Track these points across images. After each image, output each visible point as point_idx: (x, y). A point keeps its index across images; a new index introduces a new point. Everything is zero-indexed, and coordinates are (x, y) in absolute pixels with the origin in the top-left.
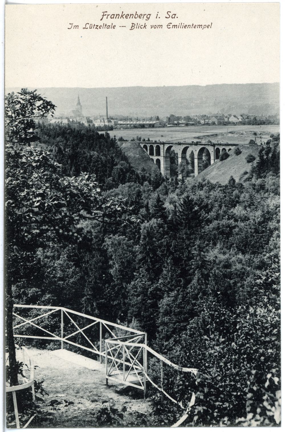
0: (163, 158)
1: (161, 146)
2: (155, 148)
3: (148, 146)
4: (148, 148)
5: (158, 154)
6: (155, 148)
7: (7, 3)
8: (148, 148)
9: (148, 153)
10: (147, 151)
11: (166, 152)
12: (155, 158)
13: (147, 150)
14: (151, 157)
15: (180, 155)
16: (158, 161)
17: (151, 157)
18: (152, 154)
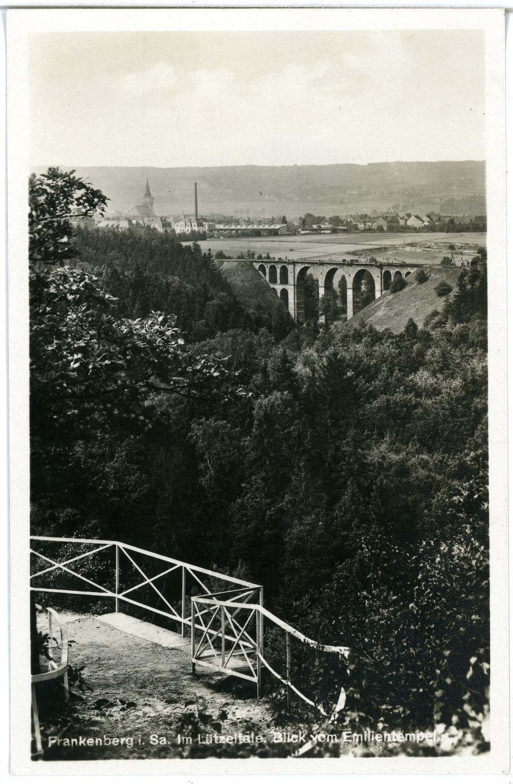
1: (290, 268)
2: (278, 271)
4: (267, 271)
5: (284, 280)
6: (278, 271)
7: (507, 11)
8: (267, 271)
9: (267, 278)
10: (265, 275)
11: (298, 278)
12: (279, 287)
13: (265, 273)
14: (272, 286)
15: (321, 283)
16: (285, 292)
17: (272, 286)
18: (273, 280)
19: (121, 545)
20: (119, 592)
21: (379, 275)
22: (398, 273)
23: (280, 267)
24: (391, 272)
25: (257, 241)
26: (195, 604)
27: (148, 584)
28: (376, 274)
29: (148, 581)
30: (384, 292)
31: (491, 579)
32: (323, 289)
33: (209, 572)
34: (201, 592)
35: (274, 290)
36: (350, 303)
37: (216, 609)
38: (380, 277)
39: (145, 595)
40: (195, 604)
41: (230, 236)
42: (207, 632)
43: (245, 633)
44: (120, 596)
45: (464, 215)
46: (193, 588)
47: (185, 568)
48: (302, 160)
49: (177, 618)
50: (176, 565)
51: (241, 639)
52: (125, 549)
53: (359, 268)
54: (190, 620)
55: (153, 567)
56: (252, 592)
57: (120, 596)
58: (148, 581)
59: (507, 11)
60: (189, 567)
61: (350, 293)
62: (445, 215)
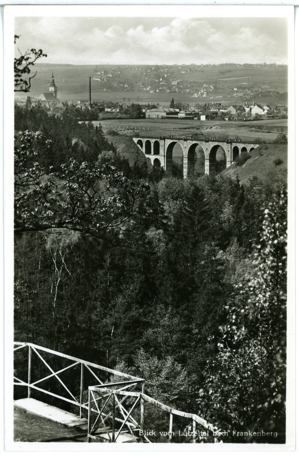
0: (163, 157)
1: (161, 142)
2: (152, 145)
3: (144, 141)
4: (144, 145)
5: (157, 152)
6: (152, 145)
7: (295, 6)
9: (144, 150)
12: (152, 157)
13: (142, 146)
14: (147, 156)
17: (147, 156)
18: (148, 152)
19: (33, 346)
20: (31, 383)
21: (230, 150)
22: (244, 149)
23: (145, 141)
24: (239, 147)
25: (138, 122)
26: (92, 392)
27: (54, 376)
28: (227, 148)
29: (54, 374)
30: (233, 163)
31: (13, 309)
32: (208, 161)
33: (101, 367)
34: (95, 383)
35: (149, 159)
36: (207, 170)
37: (108, 396)
38: (230, 151)
39: (52, 385)
40: (92, 392)
41: (151, 122)
42: (101, 415)
43: (130, 416)
44: (32, 386)
45: (16, 92)
46: (90, 381)
47: (83, 364)
48: (97, 64)
49: (77, 403)
50: (75, 362)
51: (128, 420)
52: (37, 350)
53: (171, 141)
54: (87, 405)
55: (57, 363)
56: (136, 384)
57: (32, 386)
58: (54, 374)
59: (295, 6)
60: (86, 363)
61: (207, 163)
62: (280, 105)
